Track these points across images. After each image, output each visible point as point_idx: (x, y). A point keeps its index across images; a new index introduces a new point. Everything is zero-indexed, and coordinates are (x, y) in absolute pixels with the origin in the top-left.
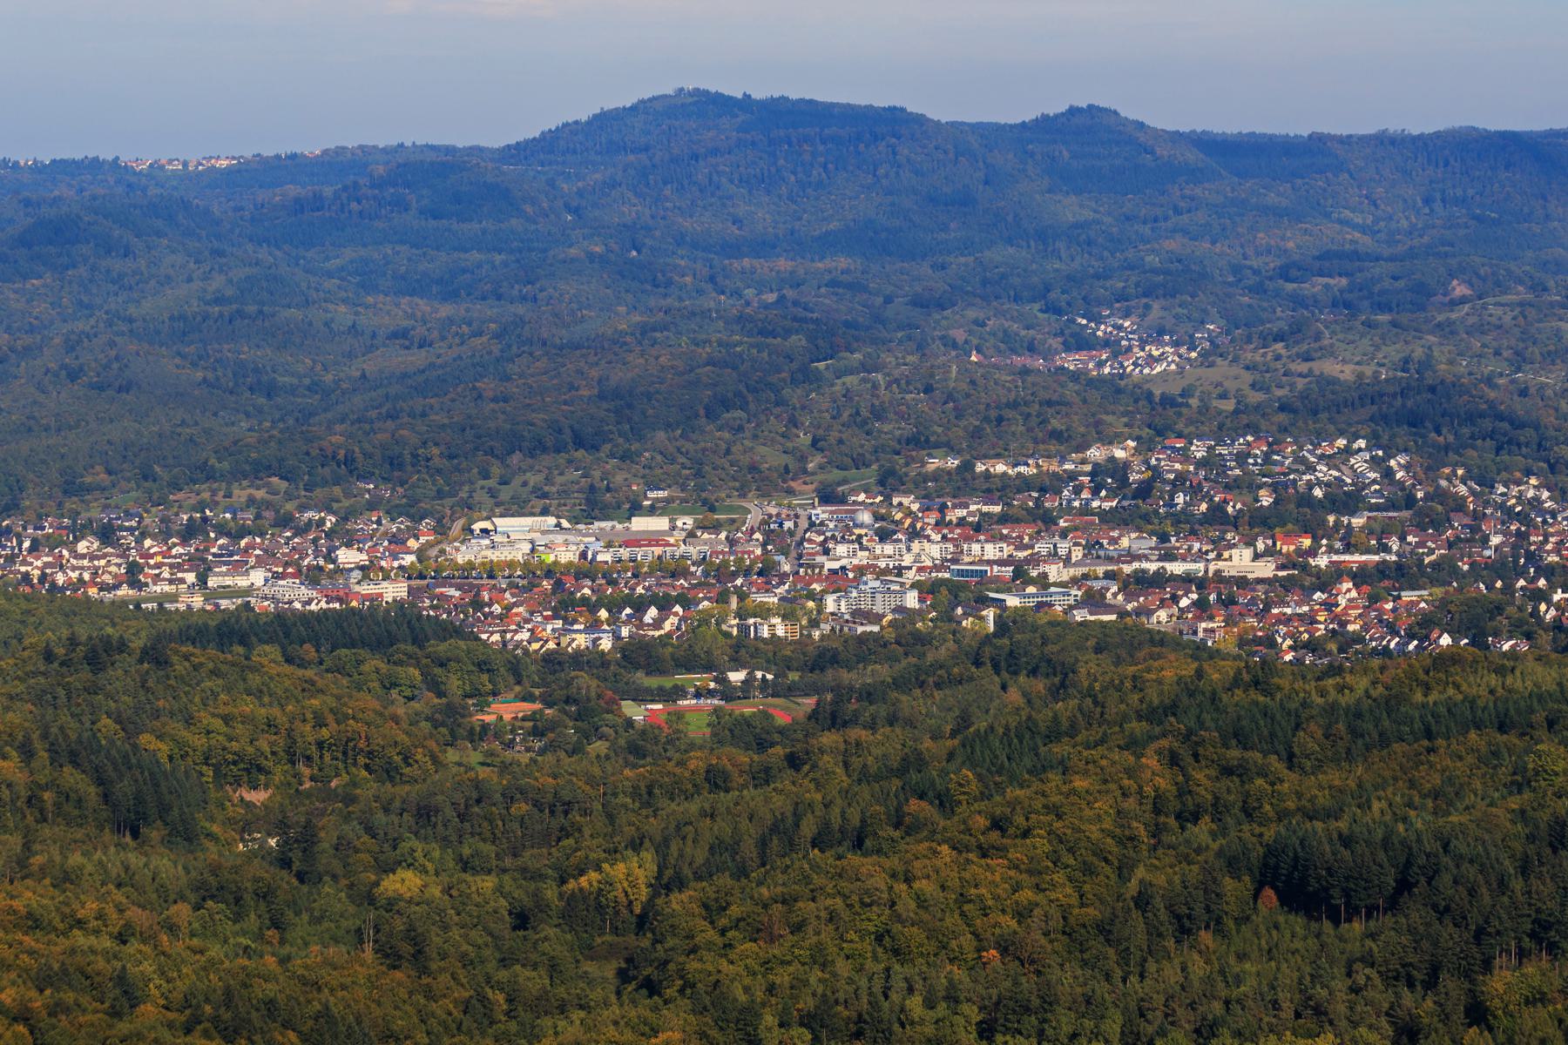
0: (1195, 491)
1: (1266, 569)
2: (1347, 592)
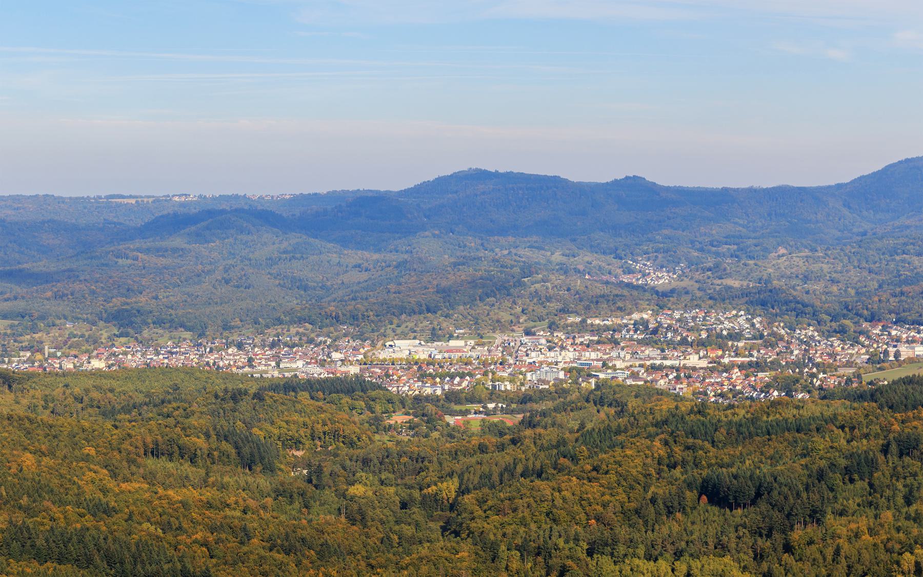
0: (675, 331)
1: (704, 363)
2: (736, 373)
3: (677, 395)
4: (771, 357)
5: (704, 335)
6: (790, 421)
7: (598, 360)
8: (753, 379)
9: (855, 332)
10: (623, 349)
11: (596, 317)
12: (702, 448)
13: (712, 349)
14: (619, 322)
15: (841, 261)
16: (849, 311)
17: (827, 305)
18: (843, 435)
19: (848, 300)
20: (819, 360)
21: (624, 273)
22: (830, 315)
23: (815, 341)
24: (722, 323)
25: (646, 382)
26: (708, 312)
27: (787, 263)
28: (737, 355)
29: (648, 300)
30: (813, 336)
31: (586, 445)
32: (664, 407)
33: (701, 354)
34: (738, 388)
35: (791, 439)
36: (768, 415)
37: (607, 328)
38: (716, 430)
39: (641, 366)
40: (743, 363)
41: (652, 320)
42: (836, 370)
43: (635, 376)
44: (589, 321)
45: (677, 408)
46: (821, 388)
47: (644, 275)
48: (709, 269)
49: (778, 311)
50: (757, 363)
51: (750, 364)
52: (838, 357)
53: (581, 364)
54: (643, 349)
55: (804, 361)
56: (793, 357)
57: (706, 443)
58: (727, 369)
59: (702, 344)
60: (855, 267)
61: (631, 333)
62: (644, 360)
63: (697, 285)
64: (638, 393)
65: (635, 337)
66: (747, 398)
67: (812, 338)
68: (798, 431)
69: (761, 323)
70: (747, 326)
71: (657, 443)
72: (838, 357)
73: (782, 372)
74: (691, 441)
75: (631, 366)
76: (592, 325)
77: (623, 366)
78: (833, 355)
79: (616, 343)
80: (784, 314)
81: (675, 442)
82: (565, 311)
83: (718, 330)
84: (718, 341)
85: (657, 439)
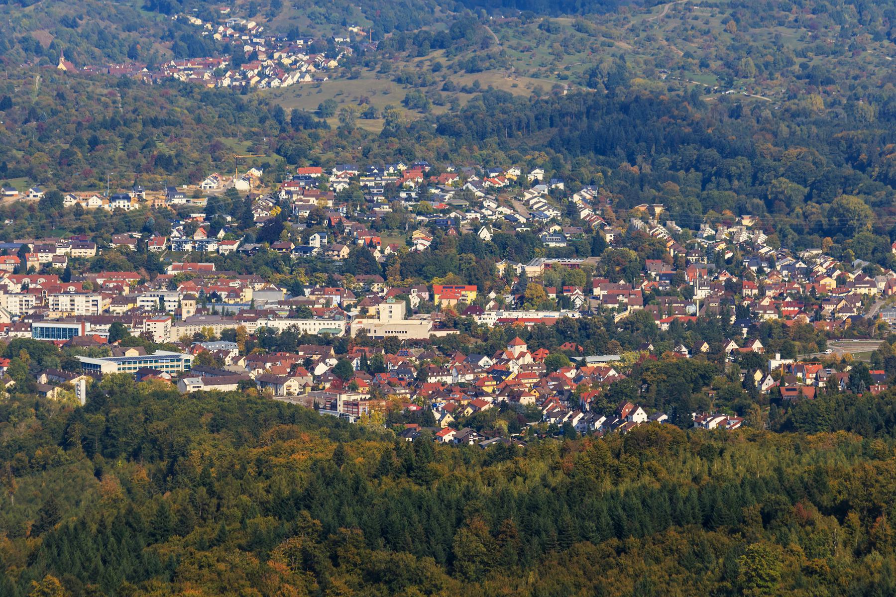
0: (335, 231)
3: (340, 424)
4: (626, 308)
5: (422, 241)
6: (682, 493)
7: (95, 319)
8: (571, 374)
9: (877, 231)
10: (173, 285)
11: (91, 187)
12: (416, 579)
13: (448, 286)
14: (161, 201)
15: (838, 17)
16: (862, 167)
17: (793, 151)
18: (841, 533)
19: (858, 134)
20: (770, 316)
21: (178, 53)
22: (803, 181)
23: (757, 259)
24: (478, 205)
25: (246, 384)
26: (435, 172)
27: (673, 24)
28: (522, 302)
29: (248, 136)
30: (751, 243)
31: (60, 573)
32: (300, 457)
33: (415, 300)
34: (524, 401)
35: (685, 548)
36: (617, 475)
37: (125, 222)
38: (459, 522)
39: (229, 336)
40: (540, 325)
41: (263, 196)
42: (822, 347)
43: (209, 366)
44: (69, 202)
45: (339, 457)
46: (775, 398)
47: (239, 60)
48: (438, 43)
49: (647, 169)
50: (584, 326)
51: (563, 330)
52: (829, 308)
53: (45, 332)
54: (236, 284)
55: (725, 320)
56: (691, 309)
57: (429, 561)
58: (495, 343)
59: (413, 271)
60: (877, 37)
61: (199, 236)
62: (240, 318)
63: (400, 92)
64: (220, 416)
65: (211, 247)
66: (554, 431)
67: (749, 248)
68: (708, 524)
69: (594, 204)
70: (551, 213)
71: (279, 564)
72: (829, 308)
73: (657, 354)
74: (381, 556)
75: (199, 337)
76: (78, 211)
77: (174, 338)
78: (811, 302)
79: (153, 267)
80: (665, 179)
81: (335, 559)
83: (465, 227)
84: (464, 259)
85: (277, 553)
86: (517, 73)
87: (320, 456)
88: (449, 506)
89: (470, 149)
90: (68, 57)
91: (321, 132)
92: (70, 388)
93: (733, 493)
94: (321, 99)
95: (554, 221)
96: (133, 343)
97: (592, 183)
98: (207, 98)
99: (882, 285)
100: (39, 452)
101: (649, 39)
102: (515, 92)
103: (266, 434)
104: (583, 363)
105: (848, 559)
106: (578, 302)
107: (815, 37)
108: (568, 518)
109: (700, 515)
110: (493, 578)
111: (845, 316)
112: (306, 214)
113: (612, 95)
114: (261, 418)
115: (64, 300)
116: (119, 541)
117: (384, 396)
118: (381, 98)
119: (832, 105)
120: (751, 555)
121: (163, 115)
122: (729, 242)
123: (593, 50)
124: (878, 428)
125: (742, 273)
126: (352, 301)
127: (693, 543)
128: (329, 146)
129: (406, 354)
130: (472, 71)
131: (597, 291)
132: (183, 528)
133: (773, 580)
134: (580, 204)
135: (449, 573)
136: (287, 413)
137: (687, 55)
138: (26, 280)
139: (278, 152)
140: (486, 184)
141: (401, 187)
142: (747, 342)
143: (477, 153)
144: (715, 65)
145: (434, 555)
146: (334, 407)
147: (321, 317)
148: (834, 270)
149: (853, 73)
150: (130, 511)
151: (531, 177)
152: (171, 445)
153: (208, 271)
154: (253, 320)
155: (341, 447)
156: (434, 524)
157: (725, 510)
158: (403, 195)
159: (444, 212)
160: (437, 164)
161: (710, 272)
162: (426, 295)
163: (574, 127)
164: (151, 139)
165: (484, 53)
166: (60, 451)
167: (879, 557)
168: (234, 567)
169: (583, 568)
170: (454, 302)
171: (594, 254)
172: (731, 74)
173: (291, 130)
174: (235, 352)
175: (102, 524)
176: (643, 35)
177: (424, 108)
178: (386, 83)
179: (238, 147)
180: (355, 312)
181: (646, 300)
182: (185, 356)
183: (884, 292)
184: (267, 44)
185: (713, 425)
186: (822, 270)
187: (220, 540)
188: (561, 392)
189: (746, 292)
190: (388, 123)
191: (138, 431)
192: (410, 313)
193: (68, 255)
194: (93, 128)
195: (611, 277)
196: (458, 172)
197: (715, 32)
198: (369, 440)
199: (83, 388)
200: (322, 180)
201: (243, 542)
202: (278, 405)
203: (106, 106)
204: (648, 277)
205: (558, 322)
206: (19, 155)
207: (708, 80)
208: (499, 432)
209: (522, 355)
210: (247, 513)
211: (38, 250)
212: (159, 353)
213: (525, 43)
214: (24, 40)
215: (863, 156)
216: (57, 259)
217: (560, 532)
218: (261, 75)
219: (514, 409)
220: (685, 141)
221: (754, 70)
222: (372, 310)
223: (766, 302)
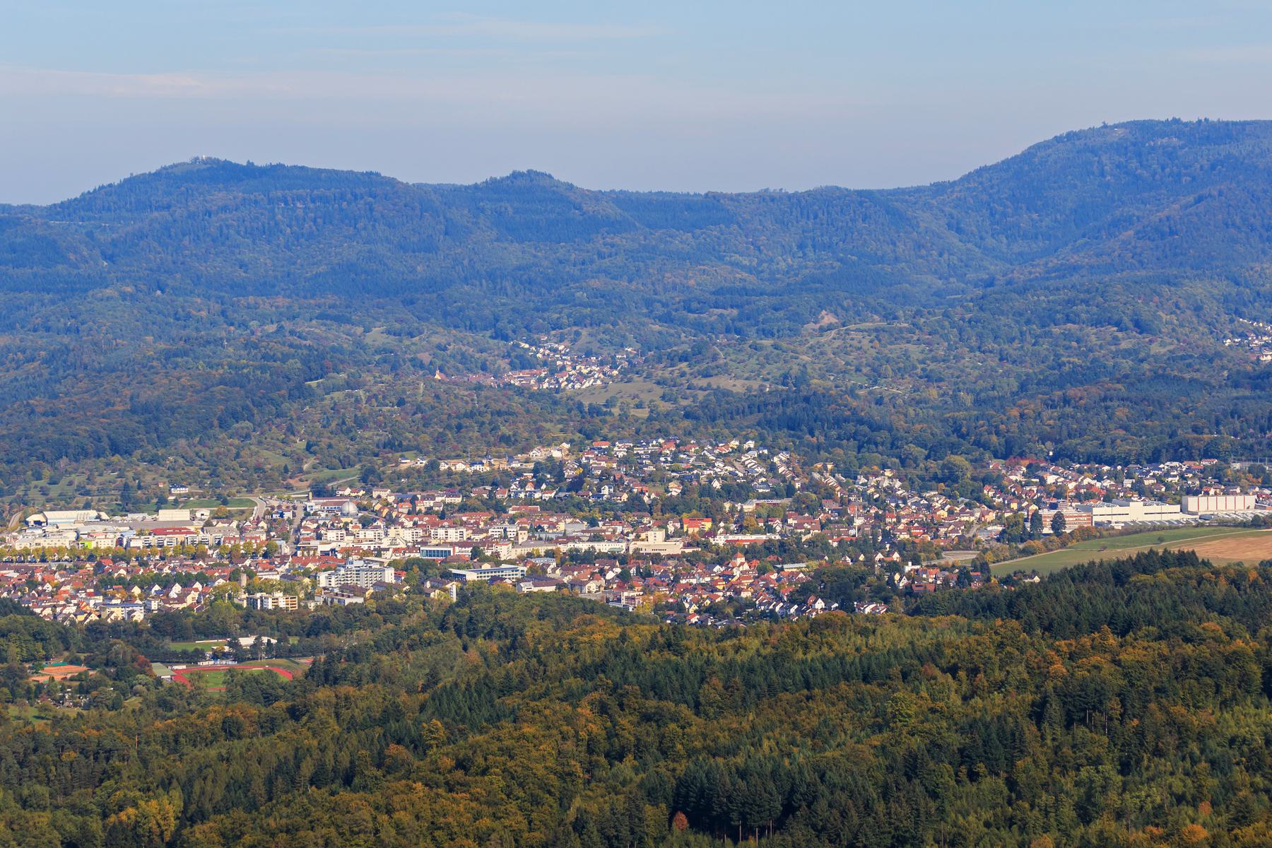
0: (618, 483)
1: (676, 547)
2: (740, 566)
3: (623, 612)
5: (675, 490)
7: (462, 544)
8: (774, 576)
9: (974, 479)
10: (512, 521)
11: (458, 457)
13: (692, 519)
14: (504, 465)
16: (962, 436)
19: (962, 414)
22: (924, 446)
23: (896, 498)
25: (560, 586)
26: (684, 443)
27: (837, 343)
28: (741, 529)
30: (891, 488)
33: (671, 529)
34: (744, 595)
36: (806, 647)
37: (480, 480)
38: (702, 680)
40: (753, 545)
42: (938, 556)
43: (537, 575)
44: (443, 467)
45: (623, 637)
46: (908, 592)
48: (684, 358)
49: (822, 439)
50: (782, 544)
51: (768, 547)
52: (943, 530)
53: (429, 553)
54: (554, 520)
55: (875, 539)
56: (852, 532)
57: (683, 707)
58: (723, 557)
59: (671, 508)
61: (529, 488)
62: (557, 541)
63: (659, 390)
64: (544, 609)
65: (537, 495)
66: (763, 615)
67: (890, 491)
68: (866, 679)
69: (788, 463)
70: (760, 470)
71: (585, 711)
72: (943, 530)
74: (652, 704)
75: (530, 555)
76: (449, 473)
77: (514, 556)
78: (931, 526)
79: (500, 509)
81: (621, 706)
82: (395, 446)
84: (705, 501)
85: (584, 702)
86: (736, 377)
87: (611, 635)
88: (696, 670)
89: (706, 428)
90: (441, 371)
91: (608, 418)
92: (445, 590)
93: (882, 659)
94: (608, 396)
95: (761, 475)
96: (486, 560)
97: (786, 449)
98: (532, 396)
99: (978, 515)
100: (426, 634)
101: (822, 353)
102: (735, 390)
103: (575, 621)
104: (782, 569)
105: (959, 702)
106: (778, 529)
107: (931, 351)
108: (774, 677)
109: (861, 674)
110: (725, 717)
111: (954, 535)
112: (599, 472)
113: (798, 391)
114: (571, 609)
115: (441, 532)
116: (479, 695)
117: (652, 593)
118: (644, 395)
119: (943, 395)
120: (895, 700)
121: (504, 408)
122: (877, 487)
123: (786, 362)
124: (976, 613)
125: (885, 507)
126: (630, 530)
127: (856, 692)
128: (613, 427)
129: (666, 565)
130: (706, 376)
131: (790, 521)
132: (522, 686)
133: (909, 716)
134: (778, 463)
135: (697, 714)
136: (589, 606)
137: (847, 364)
138: (416, 519)
139: (580, 432)
140: (717, 451)
141: (661, 454)
142: (889, 554)
143: (710, 430)
144: (865, 370)
145: (686, 702)
146: (619, 600)
147: (610, 540)
148: (945, 505)
149: (956, 374)
150: (487, 675)
151: (746, 446)
152: (513, 629)
153: (535, 511)
154: (565, 543)
155: (624, 631)
156: (686, 682)
157: (877, 671)
158: (662, 459)
159: (690, 470)
160: (684, 438)
161: (864, 508)
162: (678, 525)
163: (773, 412)
164: (495, 424)
165: (713, 364)
166: (440, 633)
167: (980, 701)
168: (555, 713)
169: (785, 710)
170: (697, 530)
171: (788, 497)
172: (876, 375)
173: (588, 417)
174: (553, 565)
175: (468, 684)
176: (818, 351)
177: (675, 401)
178: (650, 385)
179: (553, 429)
180: (631, 537)
181: (822, 527)
182: (521, 568)
183: (979, 519)
184: (572, 360)
185: (868, 610)
186: (938, 505)
187: (545, 694)
188: (767, 589)
189: (888, 520)
190: (652, 411)
191: (491, 619)
192: (668, 537)
193: (443, 502)
194: (458, 417)
195: (799, 512)
196: (698, 443)
197: (865, 348)
198: (643, 624)
199: (454, 590)
200: (609, 450)
201: (561, 695)
202: (582, 600)
203: (467, 403)
204: (824, 511)
205: (765, 542)
206: (410, 436)
207: (861, 380)
208: (727, 616)
209: (742, 564)
210: (563, 675)
211: (424, 498)
212: (504, 566)
213: (741, 357)
214: (412, 360)
215: (964, 430)
216: (437, 504)
217: (769, 686)
218: (568, 381)
219: (737, 601)
220: (846, 420)
221: (891, 373)
222: (643, 536)
223: (901, 527)
